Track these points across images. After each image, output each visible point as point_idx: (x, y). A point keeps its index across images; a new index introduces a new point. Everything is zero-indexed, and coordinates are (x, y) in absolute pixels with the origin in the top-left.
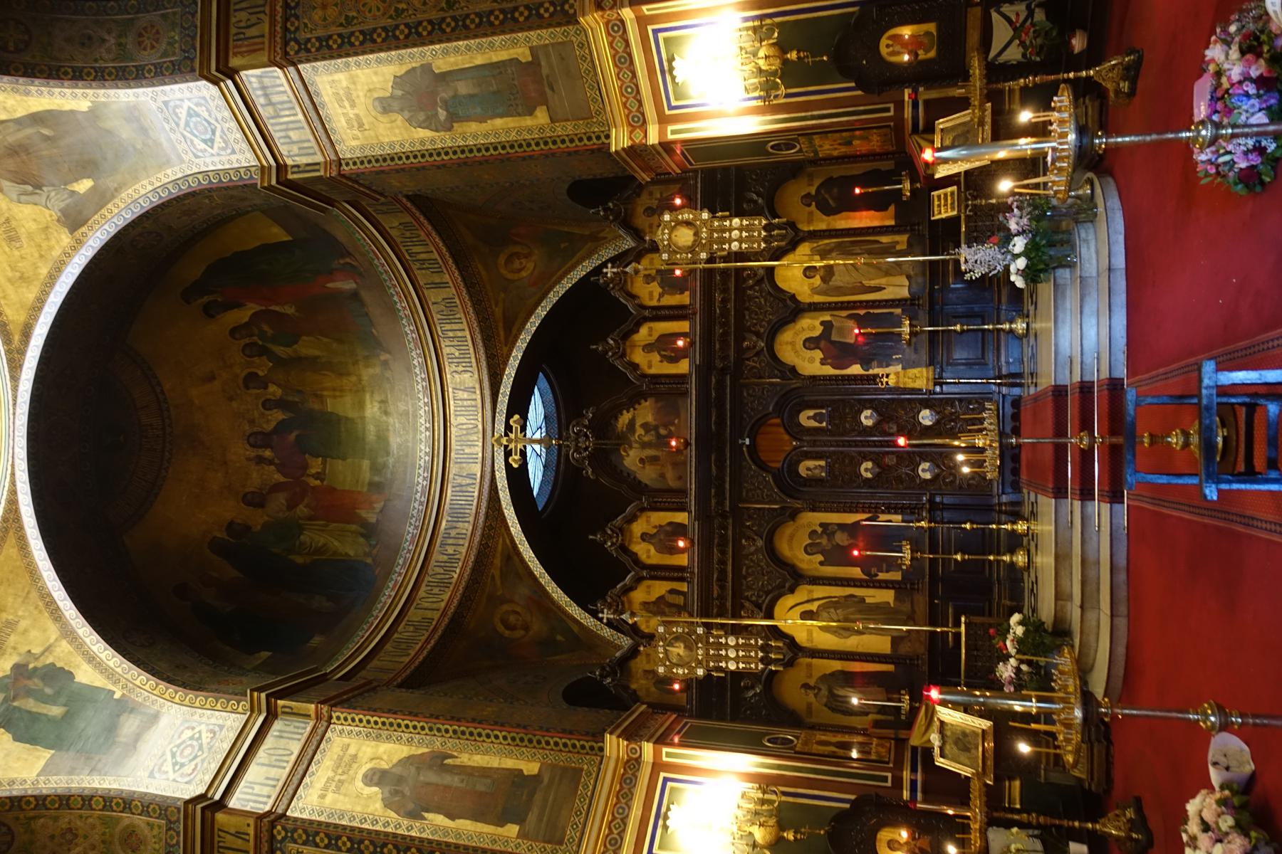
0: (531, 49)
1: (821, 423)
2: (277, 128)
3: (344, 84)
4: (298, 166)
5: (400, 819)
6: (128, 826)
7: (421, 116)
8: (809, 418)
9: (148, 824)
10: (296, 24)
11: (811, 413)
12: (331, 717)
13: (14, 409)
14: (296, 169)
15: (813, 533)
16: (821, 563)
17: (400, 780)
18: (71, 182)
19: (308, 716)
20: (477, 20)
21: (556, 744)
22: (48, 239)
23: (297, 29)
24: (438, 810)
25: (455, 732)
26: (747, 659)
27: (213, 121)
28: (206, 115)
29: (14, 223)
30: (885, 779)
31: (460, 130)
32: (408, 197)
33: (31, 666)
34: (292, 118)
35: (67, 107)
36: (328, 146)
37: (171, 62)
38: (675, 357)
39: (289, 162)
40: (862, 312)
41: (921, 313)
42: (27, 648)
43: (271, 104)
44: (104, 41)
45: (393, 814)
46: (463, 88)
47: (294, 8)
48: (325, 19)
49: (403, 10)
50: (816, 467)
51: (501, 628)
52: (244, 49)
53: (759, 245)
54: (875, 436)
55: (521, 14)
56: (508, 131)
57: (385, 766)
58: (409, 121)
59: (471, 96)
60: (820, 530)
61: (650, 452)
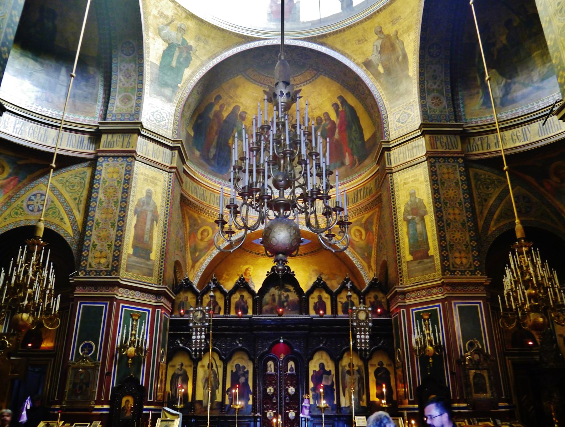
0: (433, 256)
1: (290, 371)
2: (404, 150)
3: (420, 179)
4: (390, 156)
5: (134, 206)
6: (131, 98)
7: (409, 209)
8: (291, 365)
9: (132, 106)
10: (442, 162)
11: (293, 366)
12: (171, 172)
13: (292, 39)
14: (389, 155)
15: (244, 367)
16: (232, 371)
17: (148, 204)
18: (382, 65)
19: (171, 163)
20: (442, 235)
21: (162, 266)
22: (360, 54)
23: (440, 162)
24: (138, 221)
25: (166, 224)
26: (196, 342)
27: (406, 123)
28: (408, 121)
29: (365, 43)
30: (150, 398)
31: (404, 224)
32: (380, 195)
33: (191, 52)
34: (408, 156)
35: (410, 68)
36: (398, 169)
37: (427, 111)
38: (317, 310)
39: (392, 152)
40: (335, 387)
41: (335, 412)
42: (198, 50)
43: (413, 148)
44: (435, 84)
45: (136, 203)
46: (419, 227)
47: (448, 161)
48: (443, 174)
49: (447, 205)
50: (271, 368)
51: (201, 230)
52: (432, 141)
53: (359, 347)
54: (284, 393)
55: (445, 253)
56: (404, 244)
57: (153, 197)
58: (407, 204)
59: (416, 230)
60: (246, 370)
61: (277, 298)
